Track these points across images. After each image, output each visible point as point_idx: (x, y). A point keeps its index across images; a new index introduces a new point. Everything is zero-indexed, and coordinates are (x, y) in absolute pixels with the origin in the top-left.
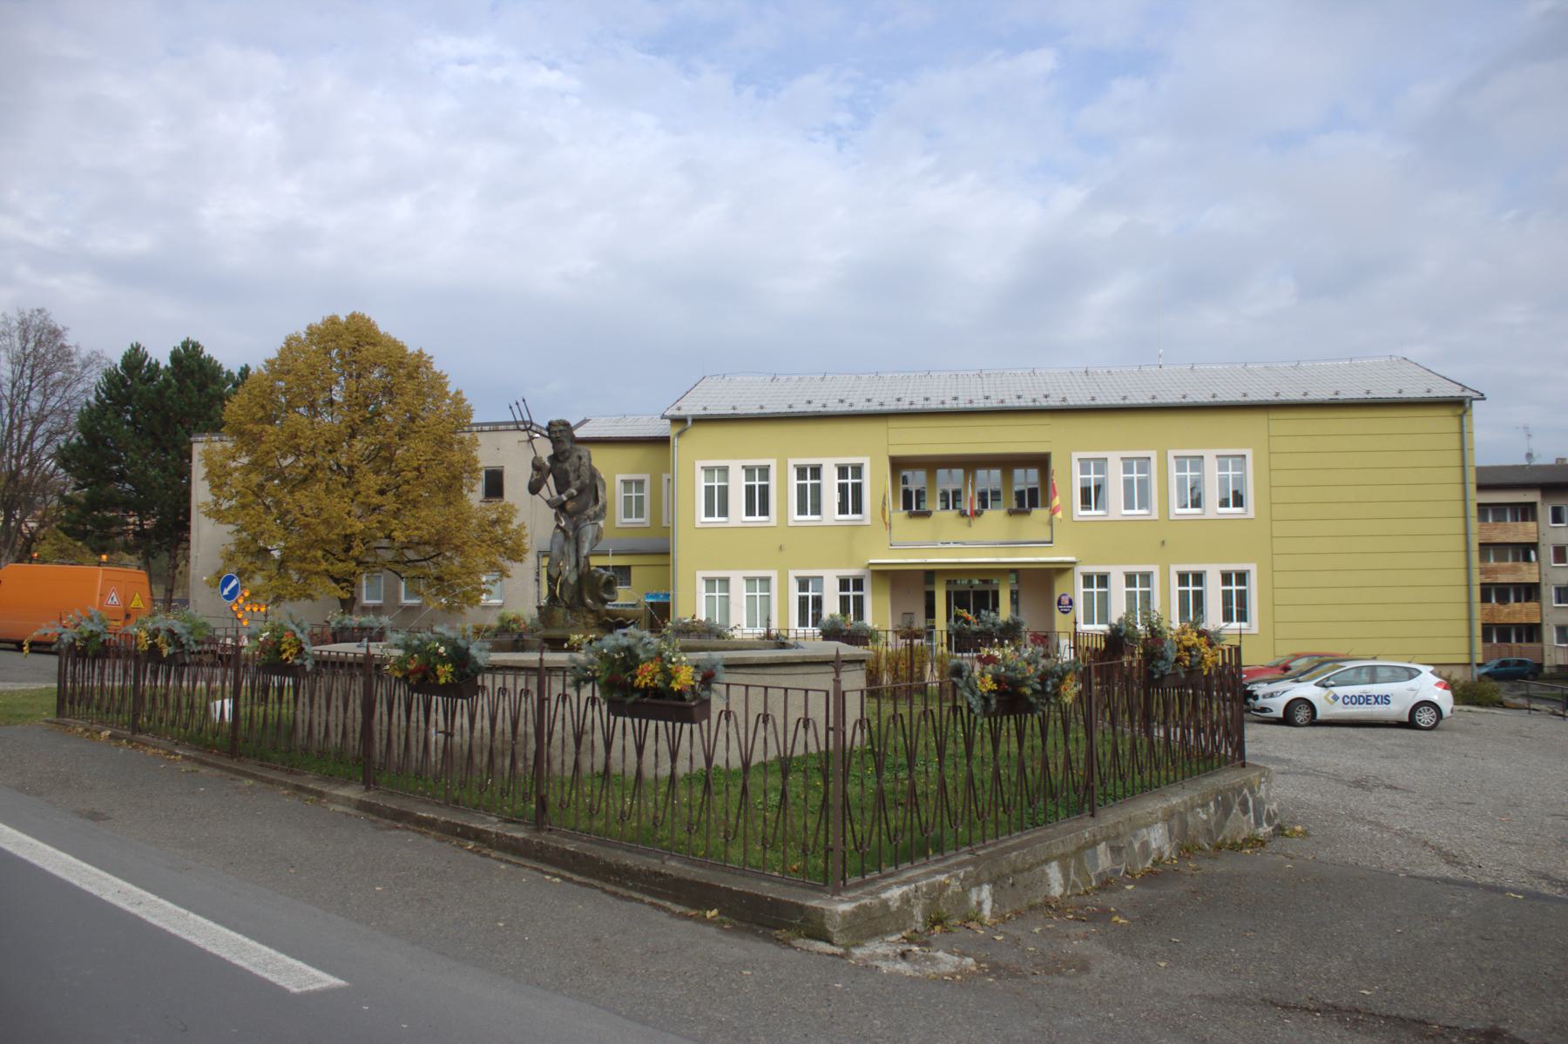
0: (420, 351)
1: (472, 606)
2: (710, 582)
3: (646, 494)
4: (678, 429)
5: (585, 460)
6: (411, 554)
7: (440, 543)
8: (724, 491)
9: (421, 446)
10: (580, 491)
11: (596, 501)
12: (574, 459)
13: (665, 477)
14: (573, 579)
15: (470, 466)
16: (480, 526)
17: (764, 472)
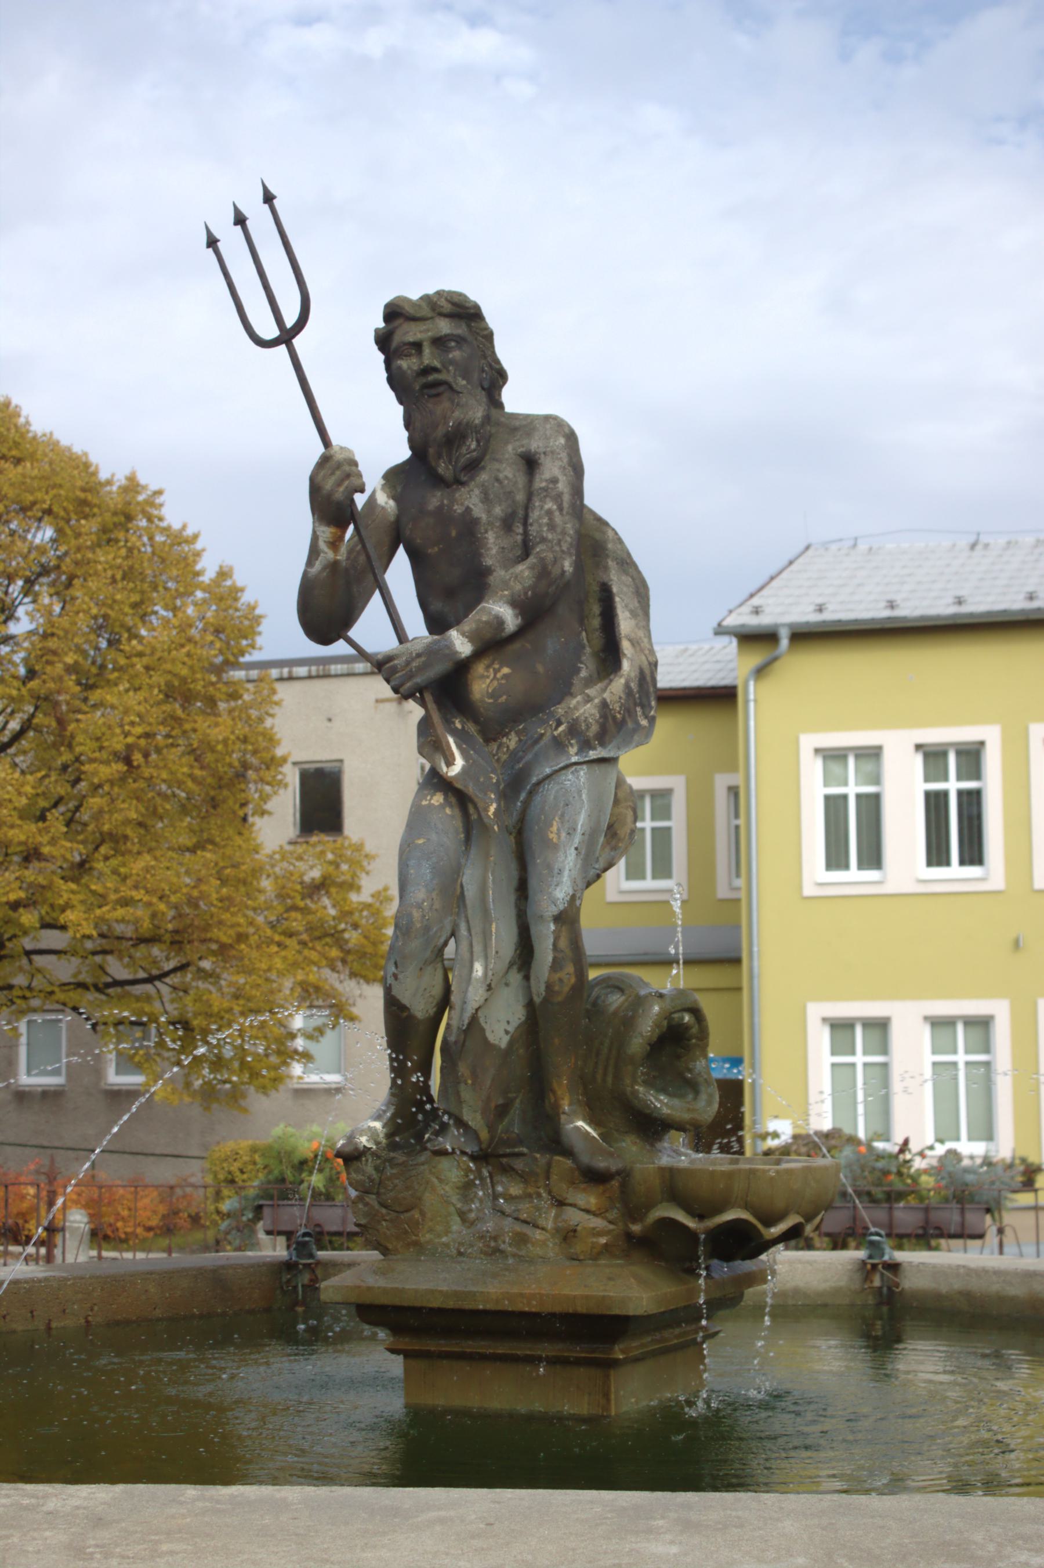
0: (132, 479)
1: (264, 1090)
2: (841, 1028)
3: (677, 823)
4: (755, 659)
5: (551, 469)
6: (117, 969)
7: (182, 940)
8: (871, 807)
9: (133, 699)
10: (535, 612)
11: (610, 656)
12: (505, 469)
13: (722, 782)
14: (503, 1022)
15: (258, 758)
16: (281, 896)
17: (971, 757)
